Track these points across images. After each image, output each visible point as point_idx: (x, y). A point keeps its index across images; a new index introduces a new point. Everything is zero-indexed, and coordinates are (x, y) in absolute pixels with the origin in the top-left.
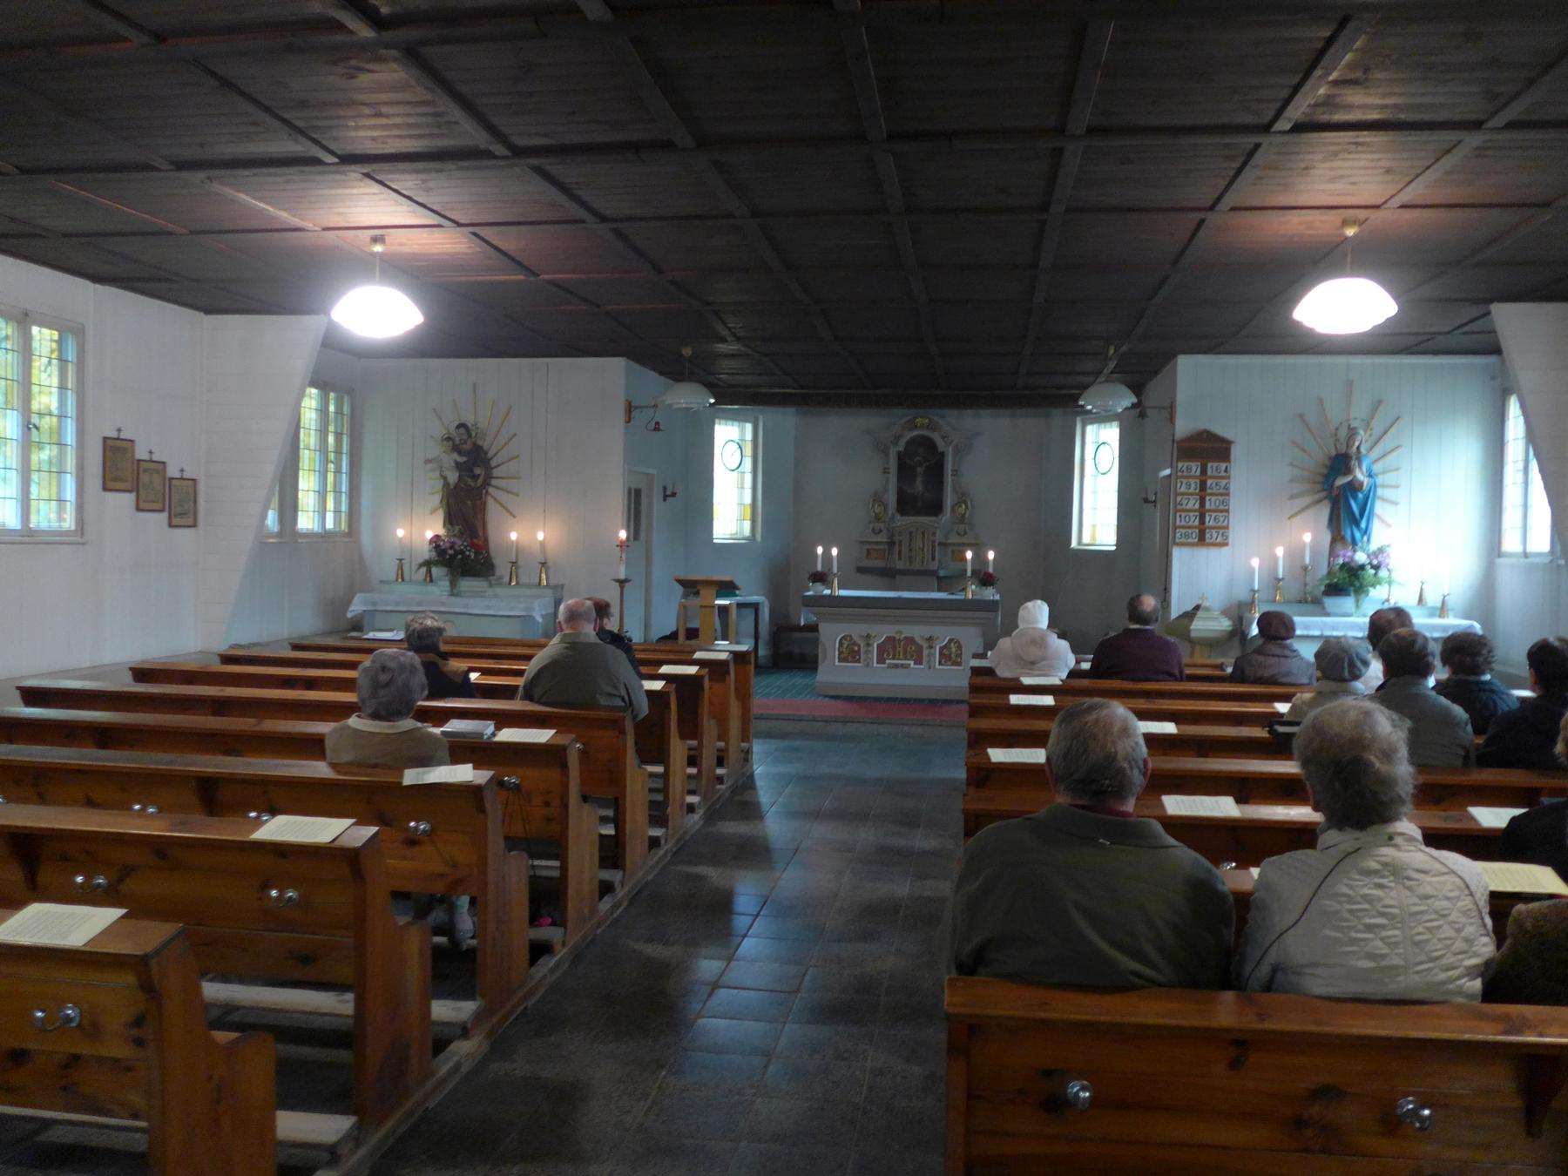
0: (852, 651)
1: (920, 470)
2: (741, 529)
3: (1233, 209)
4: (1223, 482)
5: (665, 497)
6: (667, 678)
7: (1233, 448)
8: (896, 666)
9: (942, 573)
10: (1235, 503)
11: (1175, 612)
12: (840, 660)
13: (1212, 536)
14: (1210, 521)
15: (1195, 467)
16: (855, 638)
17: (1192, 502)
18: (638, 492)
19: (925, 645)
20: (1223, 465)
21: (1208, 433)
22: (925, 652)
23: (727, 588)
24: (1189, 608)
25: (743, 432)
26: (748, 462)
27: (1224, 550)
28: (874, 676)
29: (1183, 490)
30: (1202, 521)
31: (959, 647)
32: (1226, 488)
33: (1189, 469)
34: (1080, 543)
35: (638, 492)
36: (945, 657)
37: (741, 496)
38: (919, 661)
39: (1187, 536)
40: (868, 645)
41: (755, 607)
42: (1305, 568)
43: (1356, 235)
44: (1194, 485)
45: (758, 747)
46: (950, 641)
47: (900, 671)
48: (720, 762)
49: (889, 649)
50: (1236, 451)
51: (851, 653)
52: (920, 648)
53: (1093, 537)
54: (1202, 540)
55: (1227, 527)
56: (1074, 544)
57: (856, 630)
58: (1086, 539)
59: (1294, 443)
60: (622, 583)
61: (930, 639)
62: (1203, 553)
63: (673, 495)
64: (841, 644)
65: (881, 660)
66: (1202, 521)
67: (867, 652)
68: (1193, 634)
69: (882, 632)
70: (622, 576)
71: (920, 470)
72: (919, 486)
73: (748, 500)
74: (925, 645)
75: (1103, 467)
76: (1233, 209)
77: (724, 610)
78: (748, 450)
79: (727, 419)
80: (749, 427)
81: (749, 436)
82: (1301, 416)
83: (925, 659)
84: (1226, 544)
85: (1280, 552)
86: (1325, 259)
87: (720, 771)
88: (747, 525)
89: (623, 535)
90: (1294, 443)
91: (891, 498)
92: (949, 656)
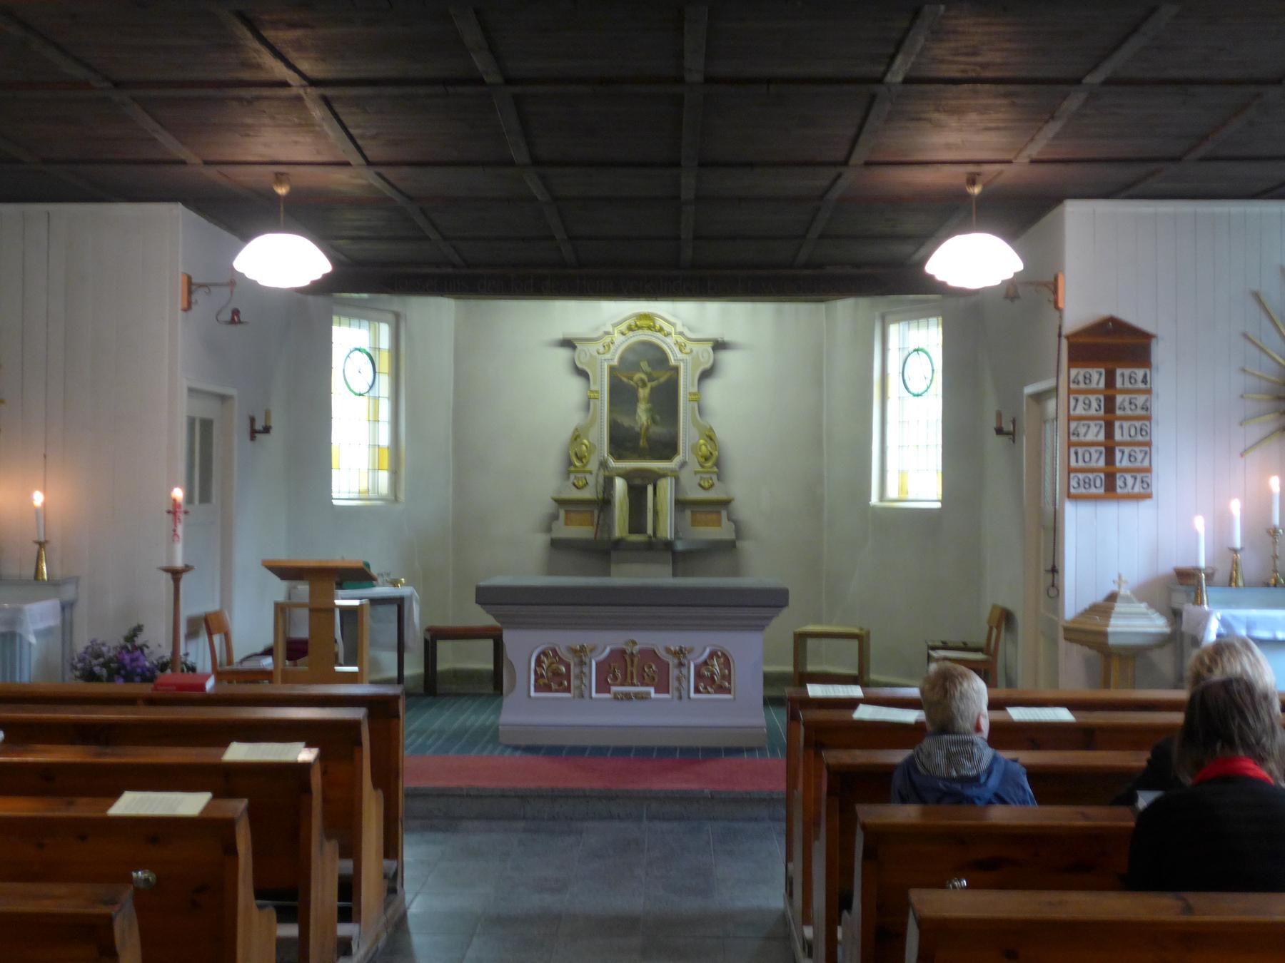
0: (556, 674)
1: (643, 393)
2: (376, 483)
3: (868, 164)
4: (1140, 399)
5: (253, 433)
6: (225, 780)
7: (1154, 342)
8: (627, 697)
9: (680, 546)
10: (1163, 434)
11: (1072, 605)
12: (537, 689)
13: (1126, 483)
14: (1121, 461)
15: (1097, 377)
16: (563, 653)
17: (1094, 429)
18: (207, 425)
19: (672, 661)
20: (1140, 373)
21: (1112, 320)
22: (673, 672)
23: (358, 576)
24: (1099, 597)
25: (376, 337)
26: (384, 384)
27: (1145, 506)
28: (595, 713)
29: (1080, 411)
30: (1110, 459)
31: (727, 663)
32: (1145, 408)
33: (1087, 379)
34: (882, 496)
35: (207, 425)
36: (706, 680)
37: (375, 434)
38: (663, 687)
39: (1088, 483)
40: (582, 663)
41: (399, 603)
42: (1273, 532)
43: (981, 194)
44: (1096, 405)
45: (413, 851)
46: (712, 655)
47: (636, 704)
48: (346, 915)
49: (619, 668)
50: (1160, 352)
51: (553, 677)
52: (664, 667)
53: (902, 488)
54: (1110, 490)
55: (1148, 470)
56: (874, 500)
57: (564, 640)
58: (892, 492)
59: (1245, 336)
60: (176, 574)
61: (680, 653)
62: (1110, 512)
63: (267, 430)
64: (539, 662)
65: (603, 686)
66: (1110, 459)
67: (580, 676)
68: (1112, 641)
69: (605, 642)
70: (179, 563)
71: (643, 393)
72: (642, 415)
73: (384, 439)
74: (672, 661)
75: (916, 385)
76: (868, 164)
77: (350, 614)
78: (384, 363)
79: (350, 316)
80: (385, 330)
81: (385, 342)
82: (1257, 296)
83: (673, 683)
84: (1148, 496)
85: (1236, 507)
86: (954, 212)
87: (344, 930)
88: (384, 478)
89: (178, 493)
90: (1245, 336)
91: (600, 435)
92: (714, 678)
